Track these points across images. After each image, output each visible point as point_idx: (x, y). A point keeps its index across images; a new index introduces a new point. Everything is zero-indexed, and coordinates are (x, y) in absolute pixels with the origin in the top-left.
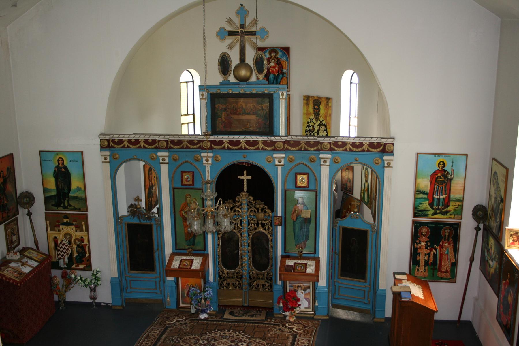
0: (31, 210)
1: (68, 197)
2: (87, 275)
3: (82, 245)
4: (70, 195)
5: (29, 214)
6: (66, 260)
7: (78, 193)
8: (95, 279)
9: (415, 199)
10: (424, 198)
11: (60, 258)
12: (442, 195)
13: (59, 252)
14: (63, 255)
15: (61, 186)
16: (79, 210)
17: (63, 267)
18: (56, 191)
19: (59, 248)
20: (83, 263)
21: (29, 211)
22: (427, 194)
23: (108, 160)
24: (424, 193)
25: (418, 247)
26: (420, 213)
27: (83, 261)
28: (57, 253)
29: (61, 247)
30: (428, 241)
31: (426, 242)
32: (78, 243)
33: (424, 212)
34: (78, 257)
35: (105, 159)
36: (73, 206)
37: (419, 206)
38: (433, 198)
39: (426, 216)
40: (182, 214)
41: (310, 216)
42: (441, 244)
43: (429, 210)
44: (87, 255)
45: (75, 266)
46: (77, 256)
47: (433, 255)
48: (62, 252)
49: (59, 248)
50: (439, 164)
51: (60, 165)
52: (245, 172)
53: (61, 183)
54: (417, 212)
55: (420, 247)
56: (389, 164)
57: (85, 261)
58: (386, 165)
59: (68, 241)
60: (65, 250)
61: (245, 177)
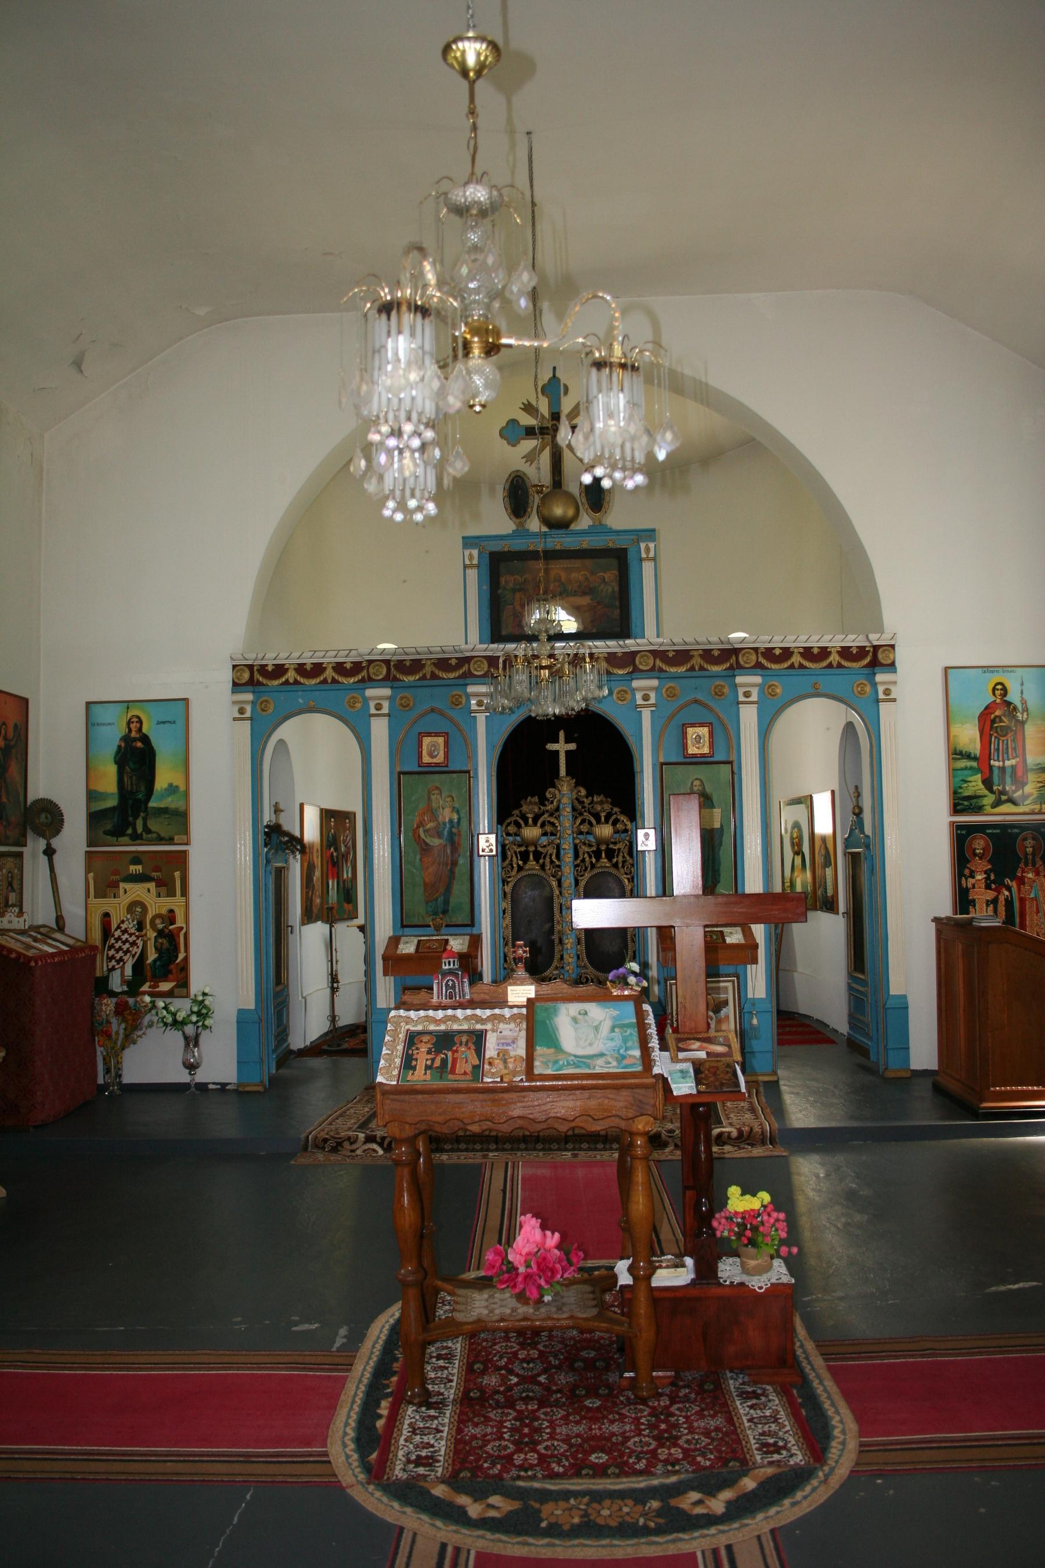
0: (55, 842)
1: (146, 807)
2: (182, 1007)
3: (170, 931)
4: (152, 804)
5: (50, 852)
6: (128, 971)
7: (170, 799)
8: (199, 1014)
9: (952, 772)
10: (971, 768)
11: (114, 966)
12: (1009, 760)
13: (112, 952)
14: (121, 959)
15: (132, 784)
16: (170, 841)
17: (119, 990)
18: (117, 796)
19: (113, 941)
20: (170, 976)
21: (49, 845)
22: (975, 759)
23: (248, 714)
24: (968, 756)
25: (970, 886)
26: (966, 803)
27: (170, 972)
28: (108, 955)
29: (118, 939)
30: (991, 870)
31: (985, 872)
32: (160, 926)
33: (974, 801)
34: (158, 963)
35: (242, 711)
36: (154, 832)
37: (961, 788)
38: (991, 767)
39: (978, 810)
40: (419, 836)
41: (722, 826)
42: (1019, 874)
43: (985, 796)
44: (181, 956)
45: (150, 987)
46: (155, 961)
47: (1004, 903)
48: (117, 951)
49: (113, 941)
50: (994, 690)
51: (133, 734)
52: (562, 734)
53: (131, 778)
54: (960, 803)
55: (974, 886)
56: (887, 692)
57: (174, 971)
58: (881, 696)
59: (135, 923)
60: (127, 945)
61: (562, 747)
